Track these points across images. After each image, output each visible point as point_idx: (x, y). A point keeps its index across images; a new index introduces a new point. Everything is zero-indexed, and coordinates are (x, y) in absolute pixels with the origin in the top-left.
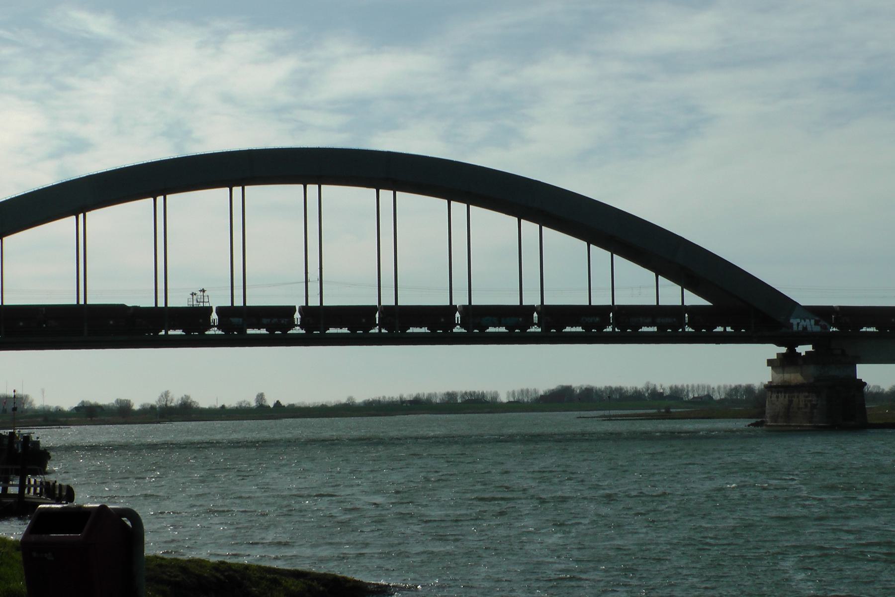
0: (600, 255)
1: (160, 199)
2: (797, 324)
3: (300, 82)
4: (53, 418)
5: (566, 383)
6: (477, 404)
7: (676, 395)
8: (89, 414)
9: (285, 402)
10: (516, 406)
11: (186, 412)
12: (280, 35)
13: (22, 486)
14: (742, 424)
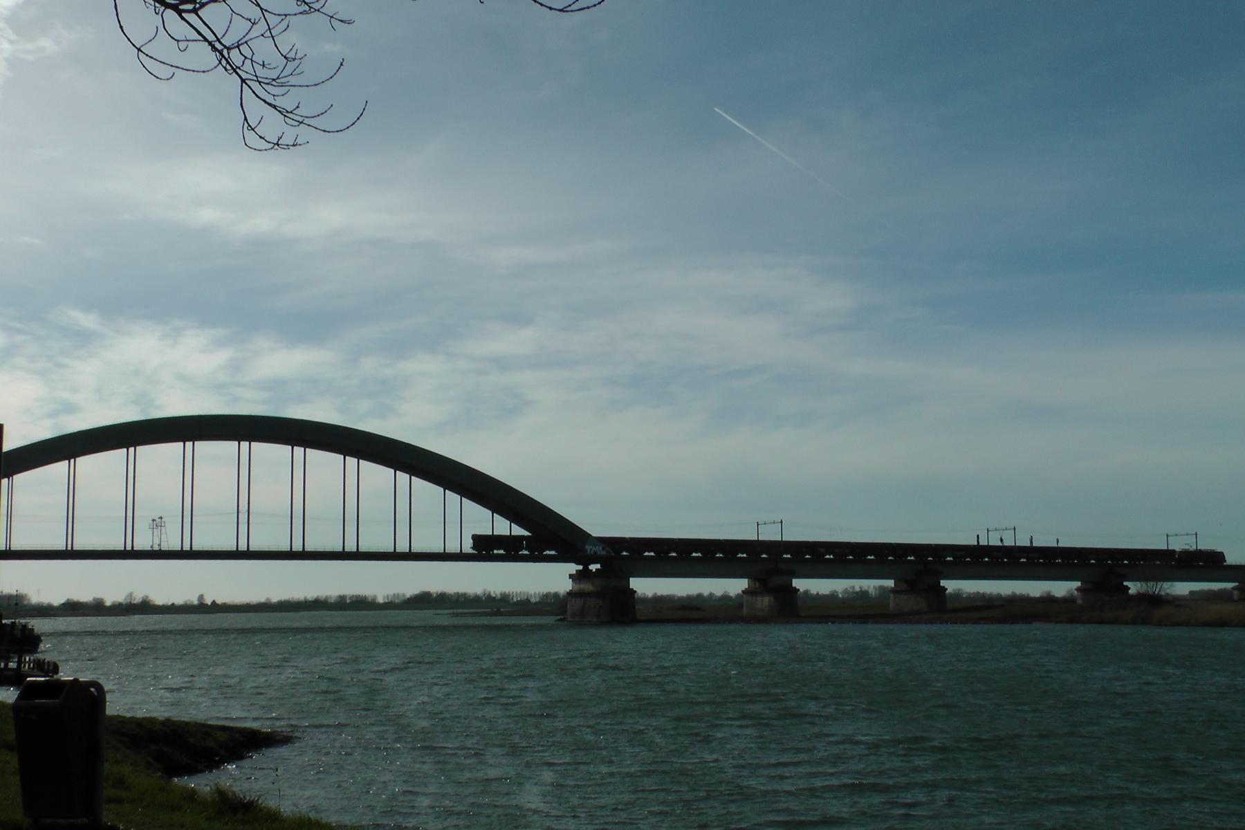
0: (453, 497)
1: (131, 450)
2: (590, 549)
3: (235, 366)
4: (45, 611)
5: (426, 590)
6: (361, 604)
7: (505, 598)
8: (72, 608)
9: (219, 601)
10: (390, 605)
11: (145, 607)
13: (19, 662)
14: (550, 620)
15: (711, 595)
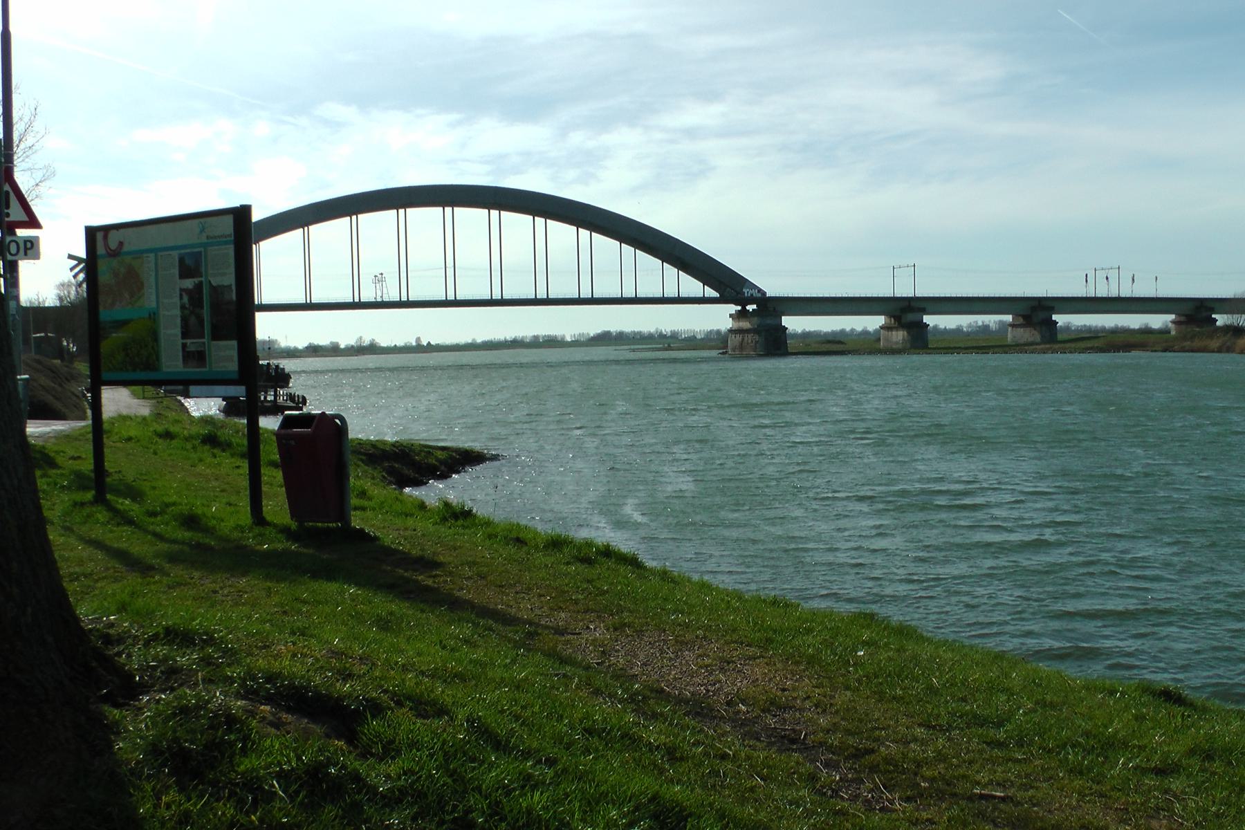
1: (354, 217)
4: (292, 353)
6: (552, 342)
7: (674, 336)
9: (433, 343)
10: (576, 343)
12: (454, 117)
13: (275, 396)
14: (714, 353)
15: (853, 330)
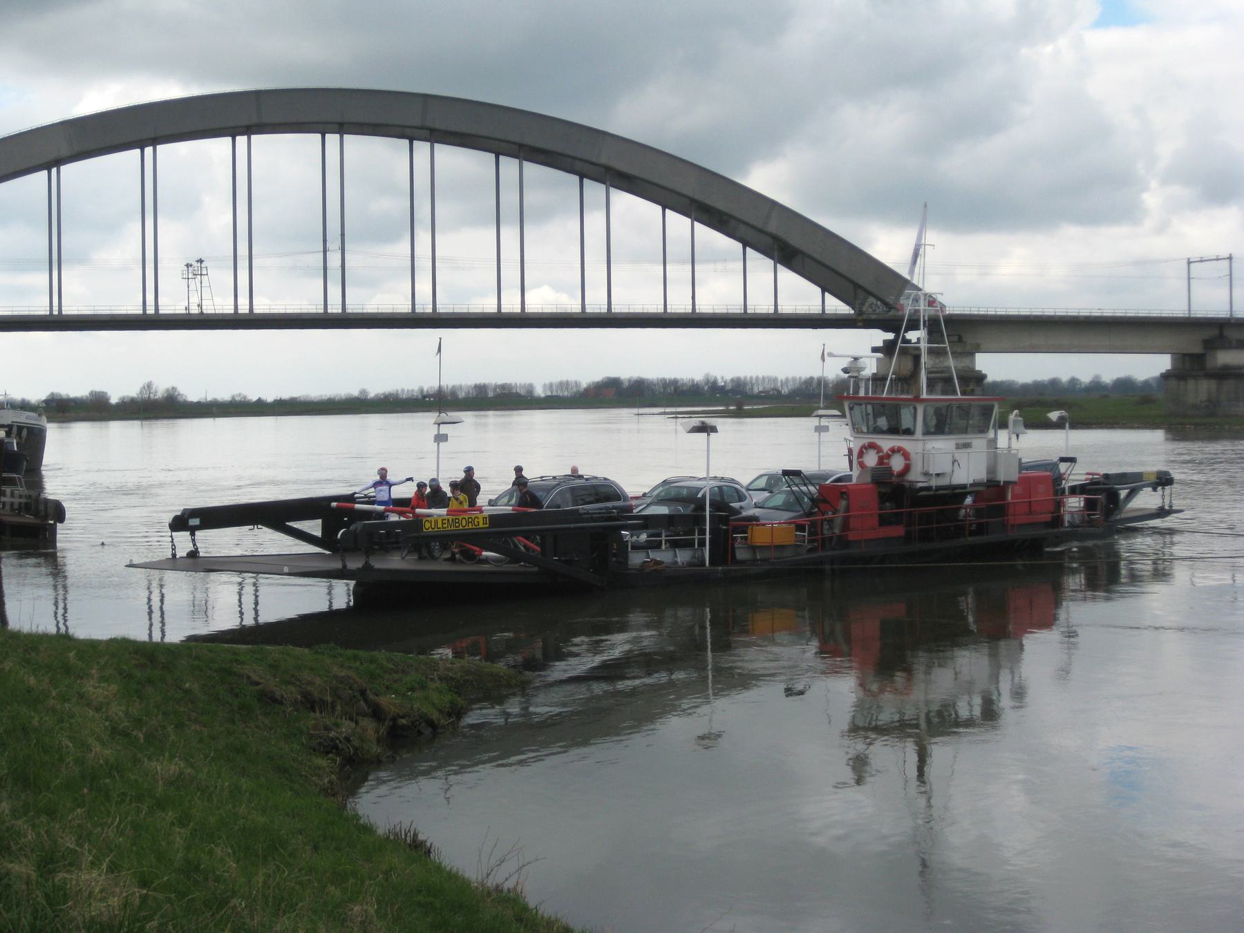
1: (149, 151)
15: (1073, 381)
